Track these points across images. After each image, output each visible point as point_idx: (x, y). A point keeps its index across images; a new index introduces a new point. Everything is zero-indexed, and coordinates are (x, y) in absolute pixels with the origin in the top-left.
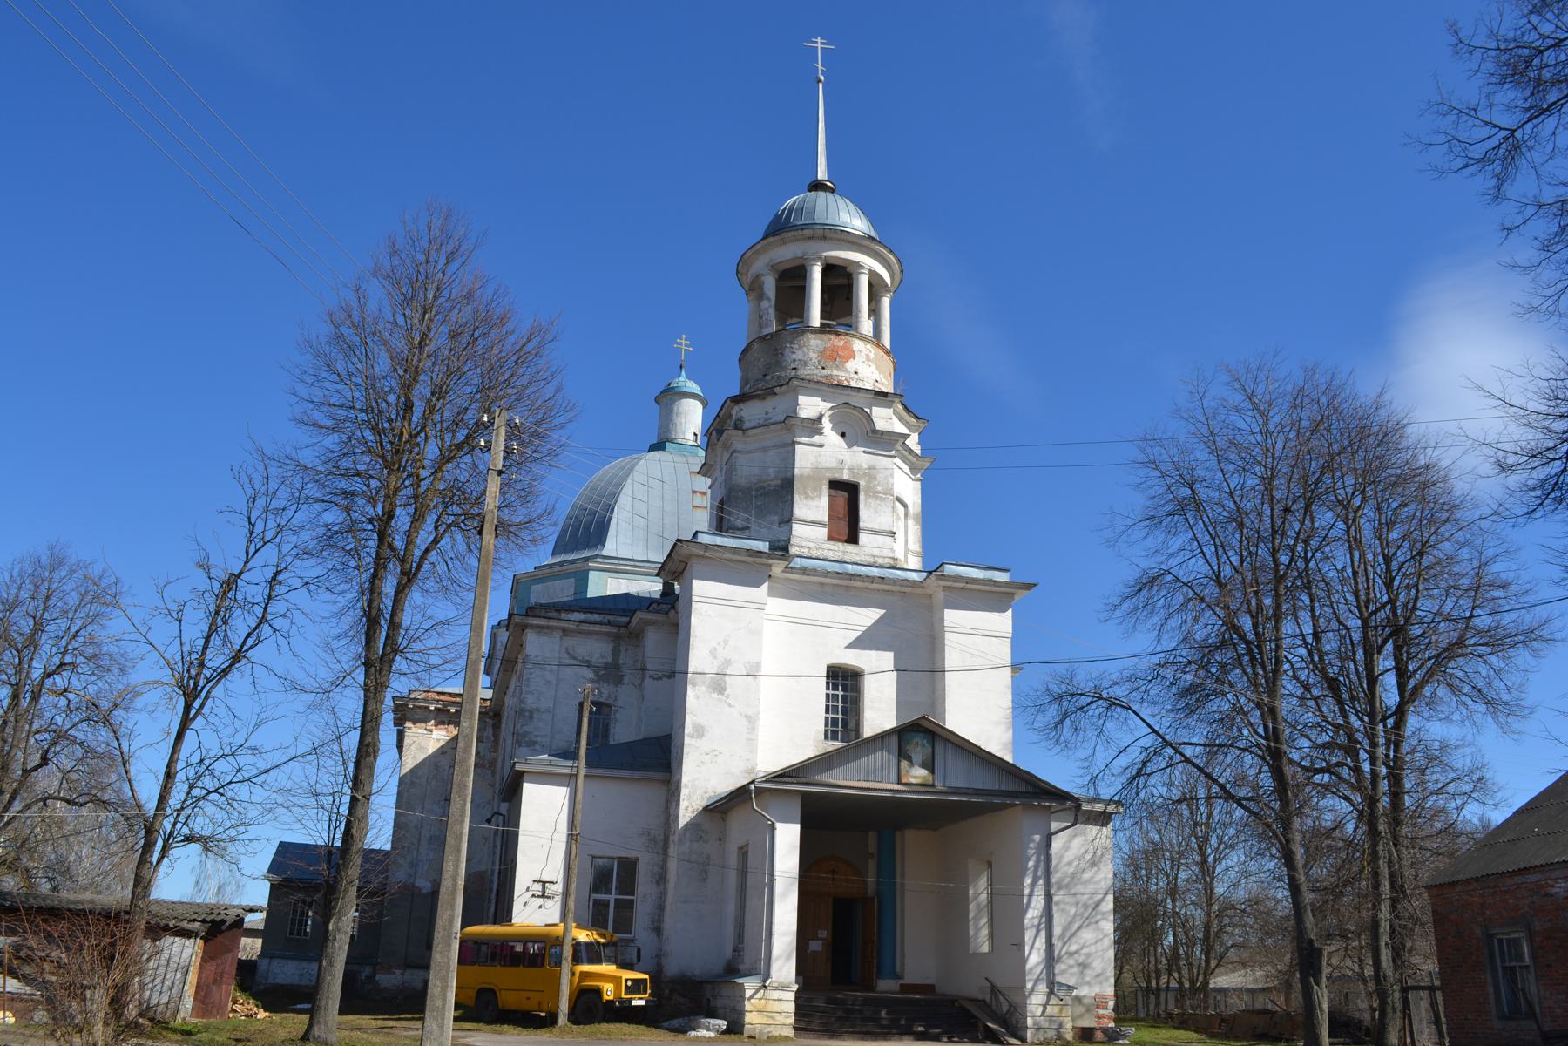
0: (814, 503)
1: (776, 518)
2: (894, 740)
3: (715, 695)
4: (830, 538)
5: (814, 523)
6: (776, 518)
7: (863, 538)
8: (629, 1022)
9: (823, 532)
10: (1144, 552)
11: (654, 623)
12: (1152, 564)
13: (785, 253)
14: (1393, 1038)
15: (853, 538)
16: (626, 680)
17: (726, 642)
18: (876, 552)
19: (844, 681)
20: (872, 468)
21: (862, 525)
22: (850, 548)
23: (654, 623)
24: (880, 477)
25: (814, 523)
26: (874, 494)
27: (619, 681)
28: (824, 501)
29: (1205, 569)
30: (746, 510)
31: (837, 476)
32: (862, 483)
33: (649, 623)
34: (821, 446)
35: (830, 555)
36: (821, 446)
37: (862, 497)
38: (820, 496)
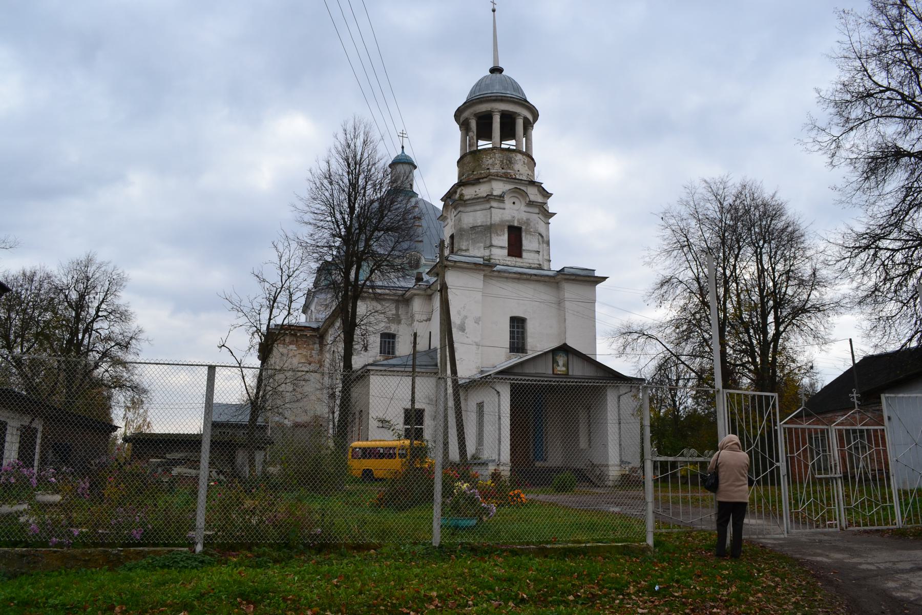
0: (501, 238)
1: (482, 245)
2: (550, 356)
4: (509, 255)
5: (501, 247)
6: (482, 245)
7: (524, 255)
8: (208, 379)
9: (506, 252)
10: (665, 267)
11: (418, 295)
12: (668, 273)
13: (483, 108)
14: (919, 591)
15: (519, 255)
18: (531, 261)
19: (518, 324)
20: (528, 219)
21: (524, 248)
22: (518, 259)
23: (418, 295)
24: (532, 224)
25: (501, 247)
26: (529, 232)
27: (399, 322)
28: (506, 237)
29: (691, 274)
30: (467, 240)
32: (524, 227)
33: (415, 295)
34: (421, 241)
35: (509, 263)
36: (421, 241)
37: (523, 234)
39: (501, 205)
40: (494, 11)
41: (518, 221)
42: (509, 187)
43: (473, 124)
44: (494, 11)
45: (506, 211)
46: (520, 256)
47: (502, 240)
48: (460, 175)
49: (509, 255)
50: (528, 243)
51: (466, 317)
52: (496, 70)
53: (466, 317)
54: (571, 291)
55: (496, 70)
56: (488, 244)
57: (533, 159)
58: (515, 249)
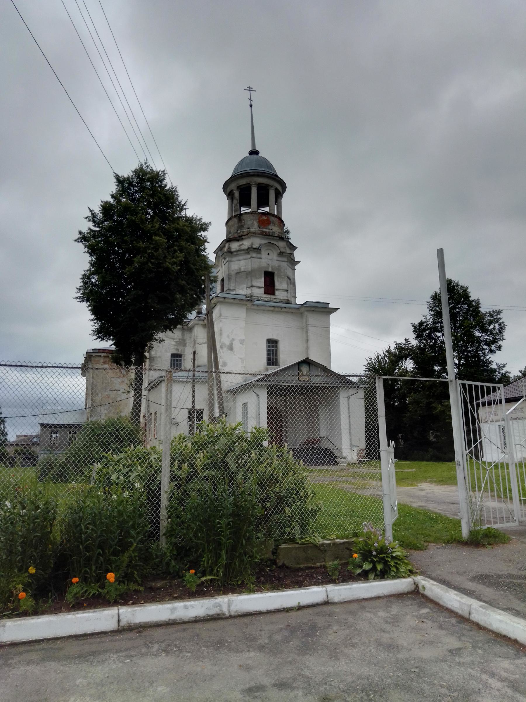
1: (245, 286)
3: (229, 351)
4: (266, 293)
7: (277, 293)
9: (263, 291)
16: (187, 344)
17: (232, 332)
18: (281, 298)
20: (279, 266)
21: (276, 288)
22: (272, 296)
27: (185, 345)
31: (267, 270)
32: (276, 272)
36: (261, 258)
37: (276, 278)
38: (261, 278)
39: (259, 256)
40: (251, 106)
41: (272, 267)
42: (264, 242)
43: (237, 194)
44: (251, 106)
45: (263, 260)
46: (273, 294)
47: (261, 282)
48: (228, 232)
49: (265, 293)
50: (279, 284)
51: (233, 340)
52: (254, 152)
53: (233, 340)
54: (313, 320)
55: (254, 152)
56: (250, 285)
57: (282, 221)
58: (270, 287)
